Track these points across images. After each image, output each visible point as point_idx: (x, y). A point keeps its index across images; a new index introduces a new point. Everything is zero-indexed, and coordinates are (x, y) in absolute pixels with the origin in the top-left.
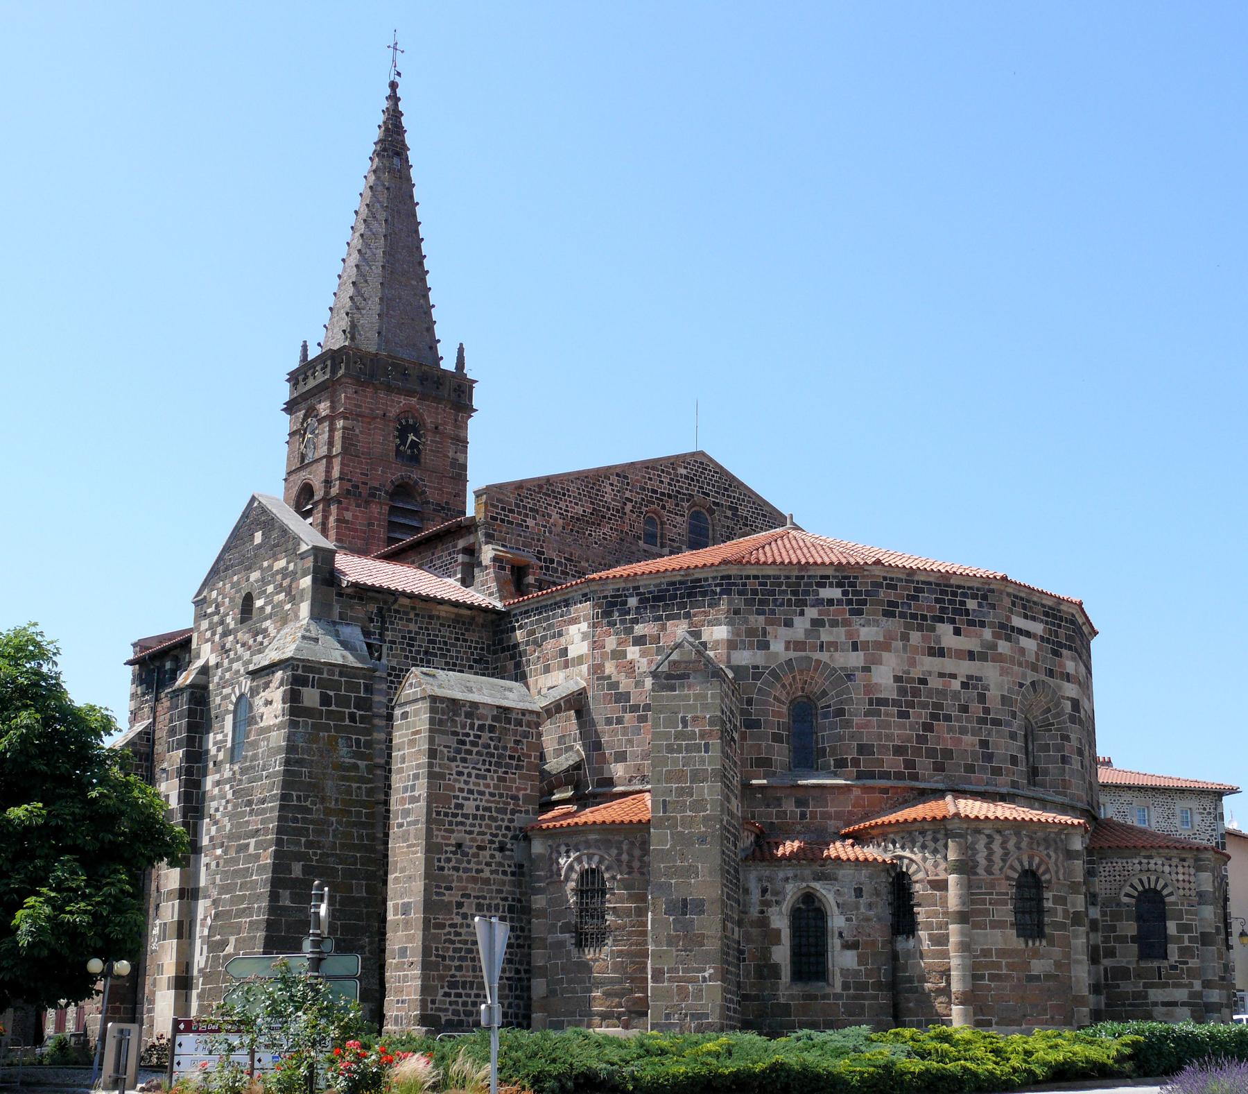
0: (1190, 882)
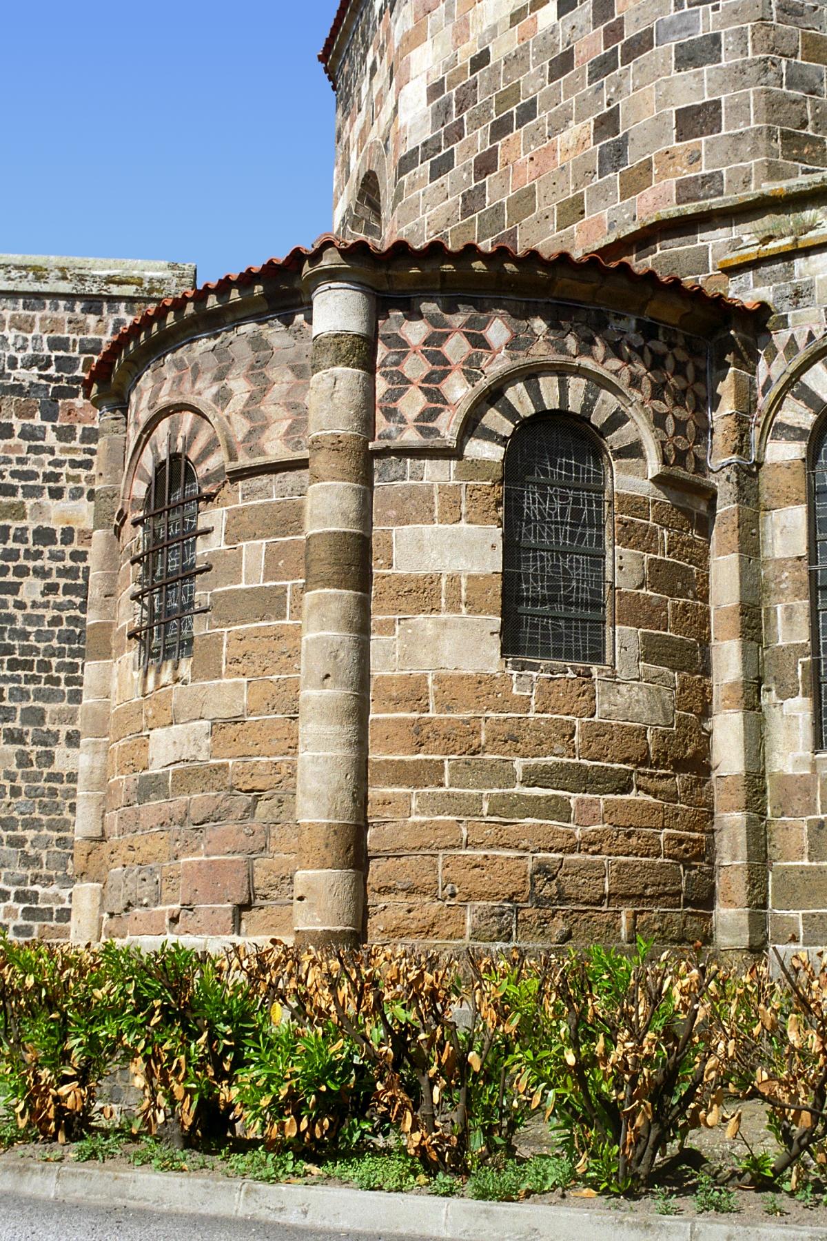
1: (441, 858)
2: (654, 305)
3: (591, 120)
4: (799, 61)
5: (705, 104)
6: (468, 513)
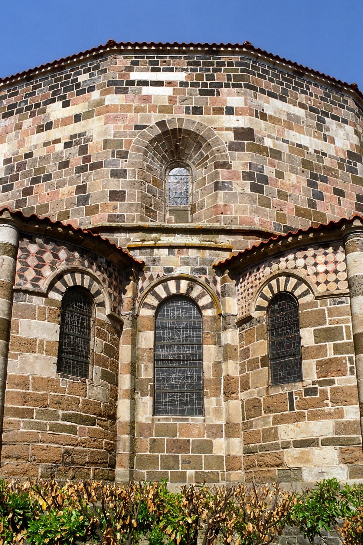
0: (336, 272)
1: (31, 446)
2: (112, 255)
3: (75, 186)
4: (151, 185)
5: (120, 191)
6: (48, 318)
